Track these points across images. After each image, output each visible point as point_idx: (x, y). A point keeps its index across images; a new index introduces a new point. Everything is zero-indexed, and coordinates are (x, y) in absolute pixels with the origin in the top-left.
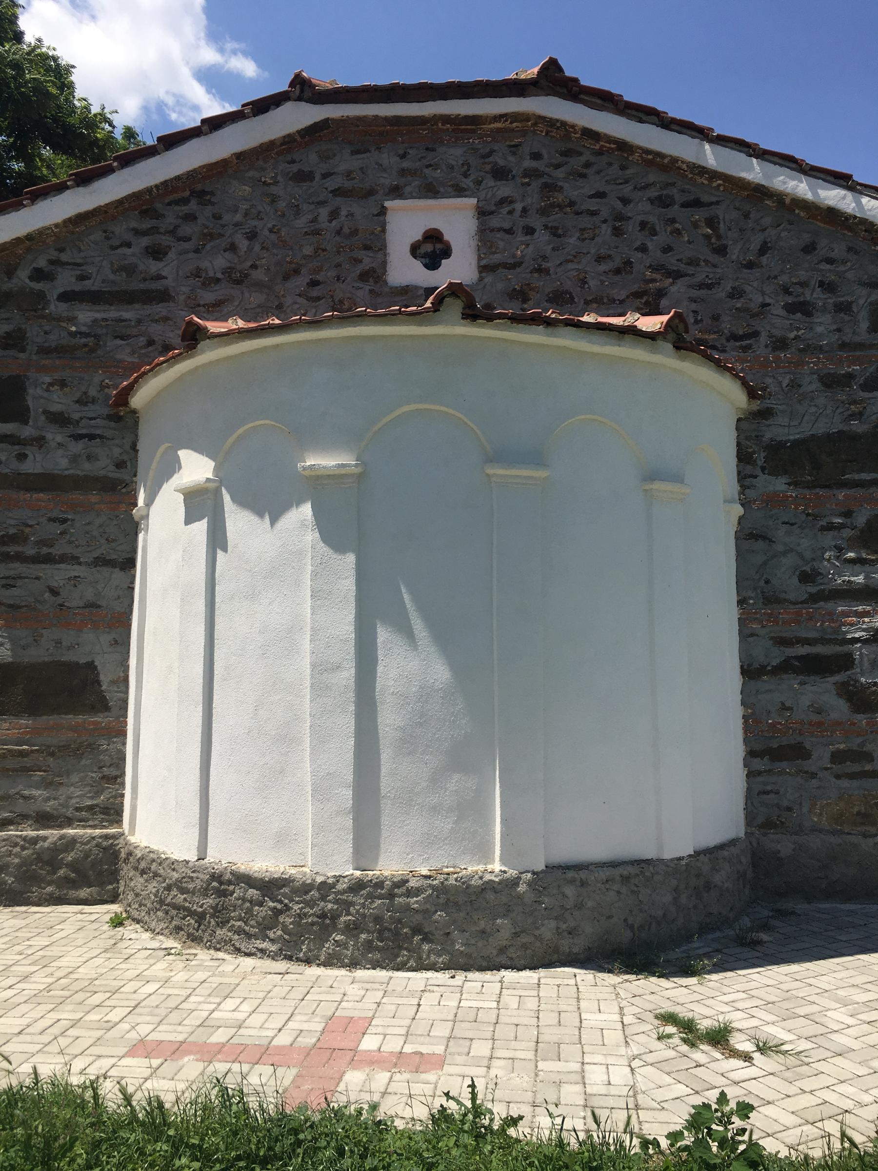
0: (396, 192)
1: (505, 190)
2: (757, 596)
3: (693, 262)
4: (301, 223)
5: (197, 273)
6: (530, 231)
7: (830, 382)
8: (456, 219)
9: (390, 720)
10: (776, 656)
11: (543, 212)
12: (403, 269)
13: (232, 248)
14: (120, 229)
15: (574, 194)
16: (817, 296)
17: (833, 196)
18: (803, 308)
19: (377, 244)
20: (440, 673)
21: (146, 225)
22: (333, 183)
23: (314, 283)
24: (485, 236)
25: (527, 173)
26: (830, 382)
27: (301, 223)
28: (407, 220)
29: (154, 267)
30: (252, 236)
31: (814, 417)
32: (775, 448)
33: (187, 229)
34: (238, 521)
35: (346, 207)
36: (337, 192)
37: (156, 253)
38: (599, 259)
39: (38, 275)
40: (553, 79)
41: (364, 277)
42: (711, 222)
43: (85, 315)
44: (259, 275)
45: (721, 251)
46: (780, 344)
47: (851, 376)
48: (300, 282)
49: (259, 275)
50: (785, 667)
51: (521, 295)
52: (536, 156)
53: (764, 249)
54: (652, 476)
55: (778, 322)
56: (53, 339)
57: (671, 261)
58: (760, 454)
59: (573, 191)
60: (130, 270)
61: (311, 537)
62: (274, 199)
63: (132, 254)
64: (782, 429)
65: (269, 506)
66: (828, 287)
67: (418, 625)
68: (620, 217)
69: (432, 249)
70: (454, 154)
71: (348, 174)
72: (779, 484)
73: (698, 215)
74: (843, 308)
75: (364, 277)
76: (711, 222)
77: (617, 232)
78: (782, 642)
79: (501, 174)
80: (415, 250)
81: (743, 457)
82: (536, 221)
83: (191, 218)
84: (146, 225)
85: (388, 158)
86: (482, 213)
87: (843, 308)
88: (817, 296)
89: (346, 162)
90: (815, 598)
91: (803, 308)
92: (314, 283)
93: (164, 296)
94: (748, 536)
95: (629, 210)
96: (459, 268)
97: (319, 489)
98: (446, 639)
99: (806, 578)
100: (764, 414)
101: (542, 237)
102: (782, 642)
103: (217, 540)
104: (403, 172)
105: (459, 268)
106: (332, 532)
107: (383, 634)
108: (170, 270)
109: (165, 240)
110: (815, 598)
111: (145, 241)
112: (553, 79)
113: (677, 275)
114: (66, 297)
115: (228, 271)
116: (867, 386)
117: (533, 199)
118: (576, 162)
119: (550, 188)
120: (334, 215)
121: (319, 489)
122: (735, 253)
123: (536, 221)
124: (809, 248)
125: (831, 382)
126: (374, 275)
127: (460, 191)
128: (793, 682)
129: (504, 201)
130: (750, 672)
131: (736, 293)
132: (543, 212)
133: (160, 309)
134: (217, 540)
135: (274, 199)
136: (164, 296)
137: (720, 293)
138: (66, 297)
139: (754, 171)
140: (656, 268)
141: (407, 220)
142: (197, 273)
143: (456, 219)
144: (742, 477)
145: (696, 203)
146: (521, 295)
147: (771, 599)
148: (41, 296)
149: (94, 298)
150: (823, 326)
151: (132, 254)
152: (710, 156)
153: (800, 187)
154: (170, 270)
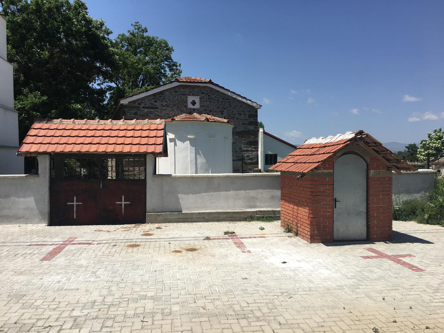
0: (189, 95)
1: (203, 96)
2: (234, 151)
3: (227, 107)
4: (176, 98)
5: (162, 105)
6: (207, 101)
7: (243, 124)
8: (197, 99)
9: (199, 166)
10: (237, 158)
11: (208, 99)
12: (190, 106)
13: (167, 101)
14: (150, 98)
15: (212, 97)
16: (242, 113)
17: (244, 100)
18: (240, 114)
19: (186, 102)
20: (204, 161)
21: (154, 97)
22: (180, 93)
23: (178, 107)
24: (201, 102)
25: (206, 93)
26: (243, 124)
27: (176, 98)
28: (190, 99)
29: (156, 104)
30: (169, 100)
31: (241, 129)
32: (237, 132)
33: (160, 98)
34: (178, 142)
35: (182, 96)
36: (181, 94)
37: (156, 102)
38: (216, 106)
39: (139, 104)
40: (210, 82)
41: (185, 107)
42: (229, 102)
43: (146, 110)
44: (170, 106)
45: (231, 106)
46: (237, 119)
47: (245, 123)
48: (176, 107)
49: (170, 106)
50: (237, 160)
51: (206, 110)
52: (207, 91)
53: (236, 106)
54: (225, 138)
55: (237, 116)
56: (141, 114)
57: (224, 107)
58: (235, 133)
59: (212, 96)
60: (152, 104)
61: (189, 145)
62: (172, 95)
63: (152, 102)
64: (238, 130)
65: (183, 140)
66: (243, 111)
67: (202, 155)
68: (218, 100)
69: (194, 103)
70: (197, 90)
71: (182, 92)
72: (237, 137)
73: (228, 101)
74: (245, 114)
75: (185, 107)
76: (229, 102)
77: (218, 102)
78: (237, 157)
79: (203, 93)
80: (191, 103)
81: (233, 133)
82: (208, 100)
83: (160, 97)
84: (154, 97)
85: (188, 90)
86: (200, 98)
87: (245, 114)
88: (242, 113)
89: (182, 90)
90: (241, 151)
91: (240, 114)
92: (178, 107)
93: (157, 108)
94: (234, 144)
95: (219, 100)
96: (197, 106)
97: (190, 140)
98: (205, 157)
99: (240, 149)
100: (236, 128)
101: (208, 102)
102: (237, 157)
103: (175, 145)
104: (190, 92)
105: (197, 106)
106: (192, 144)
107: (198, 156)
108: (158, 104)
109: (157, 100)
110: (241, 151)
111: (154, 100)
112: (210, 82)
113: (225, 109)
114: (143, 107)
115: (166, 105)
116: (247, 125)
117: (207, 97)
118: (213, 92)
119: (209, 96)
120: (181, 97)
121: (190, 140)
122: (232, 106)
123: (208, 100)
124: (241, 106)
125: (243, 124)
126: (186, 106)
127: (197, 95)
128: (238, 161)
129: (203, 97)
130: (233, 160)
131: (232, 112)
132: (208, 99)
133: (157, 110)
134: (175, 145)
135: (172, 95)
136: (157, 108)
137: (230, 112)
138: (143, 107)
139: (235, 96)
140: (223, 108)
141: (190, 99)
142: (162, 105)
143: (197, 99)
144: (233, 136)
145: (227, 99)
146: (206, 110)
147: (236, 151)
148: (139, 107)
149: (147, 108)
150: (242, 116)
151: (152, 102)
152: (230, 94)
153: (240, 99)
154: (158, 104)
